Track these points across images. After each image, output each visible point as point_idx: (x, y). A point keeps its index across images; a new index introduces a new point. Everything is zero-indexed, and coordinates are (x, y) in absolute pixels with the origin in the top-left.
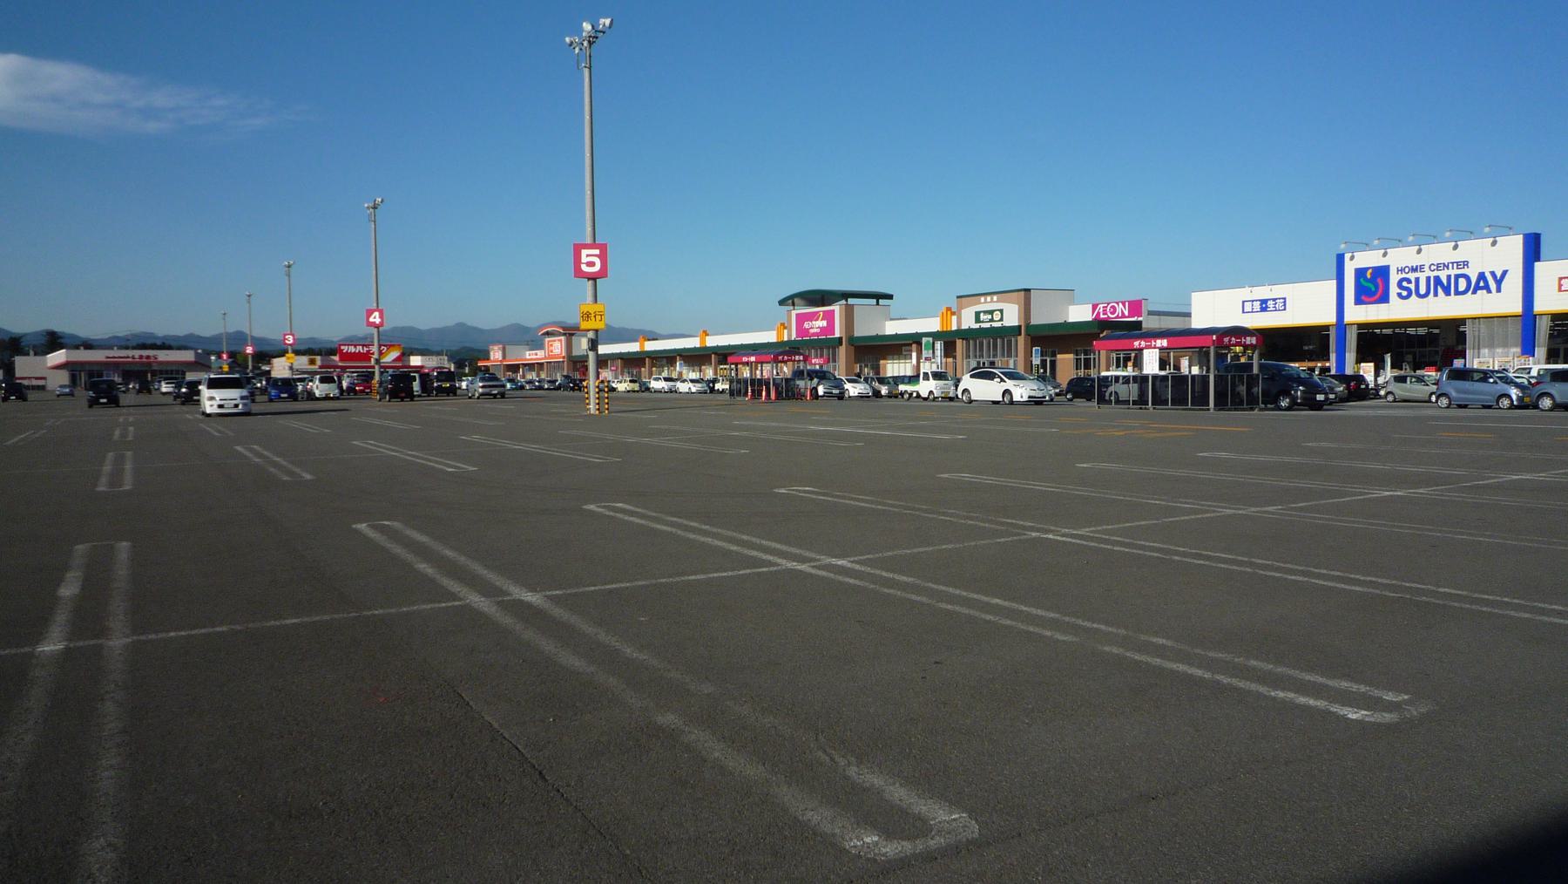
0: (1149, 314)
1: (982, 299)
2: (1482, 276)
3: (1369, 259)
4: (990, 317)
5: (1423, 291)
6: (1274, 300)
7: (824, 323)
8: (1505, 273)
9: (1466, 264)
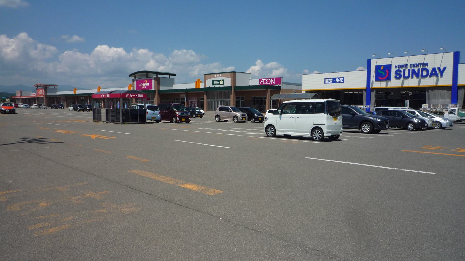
0: (283, 84)
1: (215, 76)
2: (434, 69)
3: (383, 62)
4: (218, 83)
5: (406, 75)
6: (339, 78)
7: (148, 84)
8: (445, 68)
9: (427, 64)
